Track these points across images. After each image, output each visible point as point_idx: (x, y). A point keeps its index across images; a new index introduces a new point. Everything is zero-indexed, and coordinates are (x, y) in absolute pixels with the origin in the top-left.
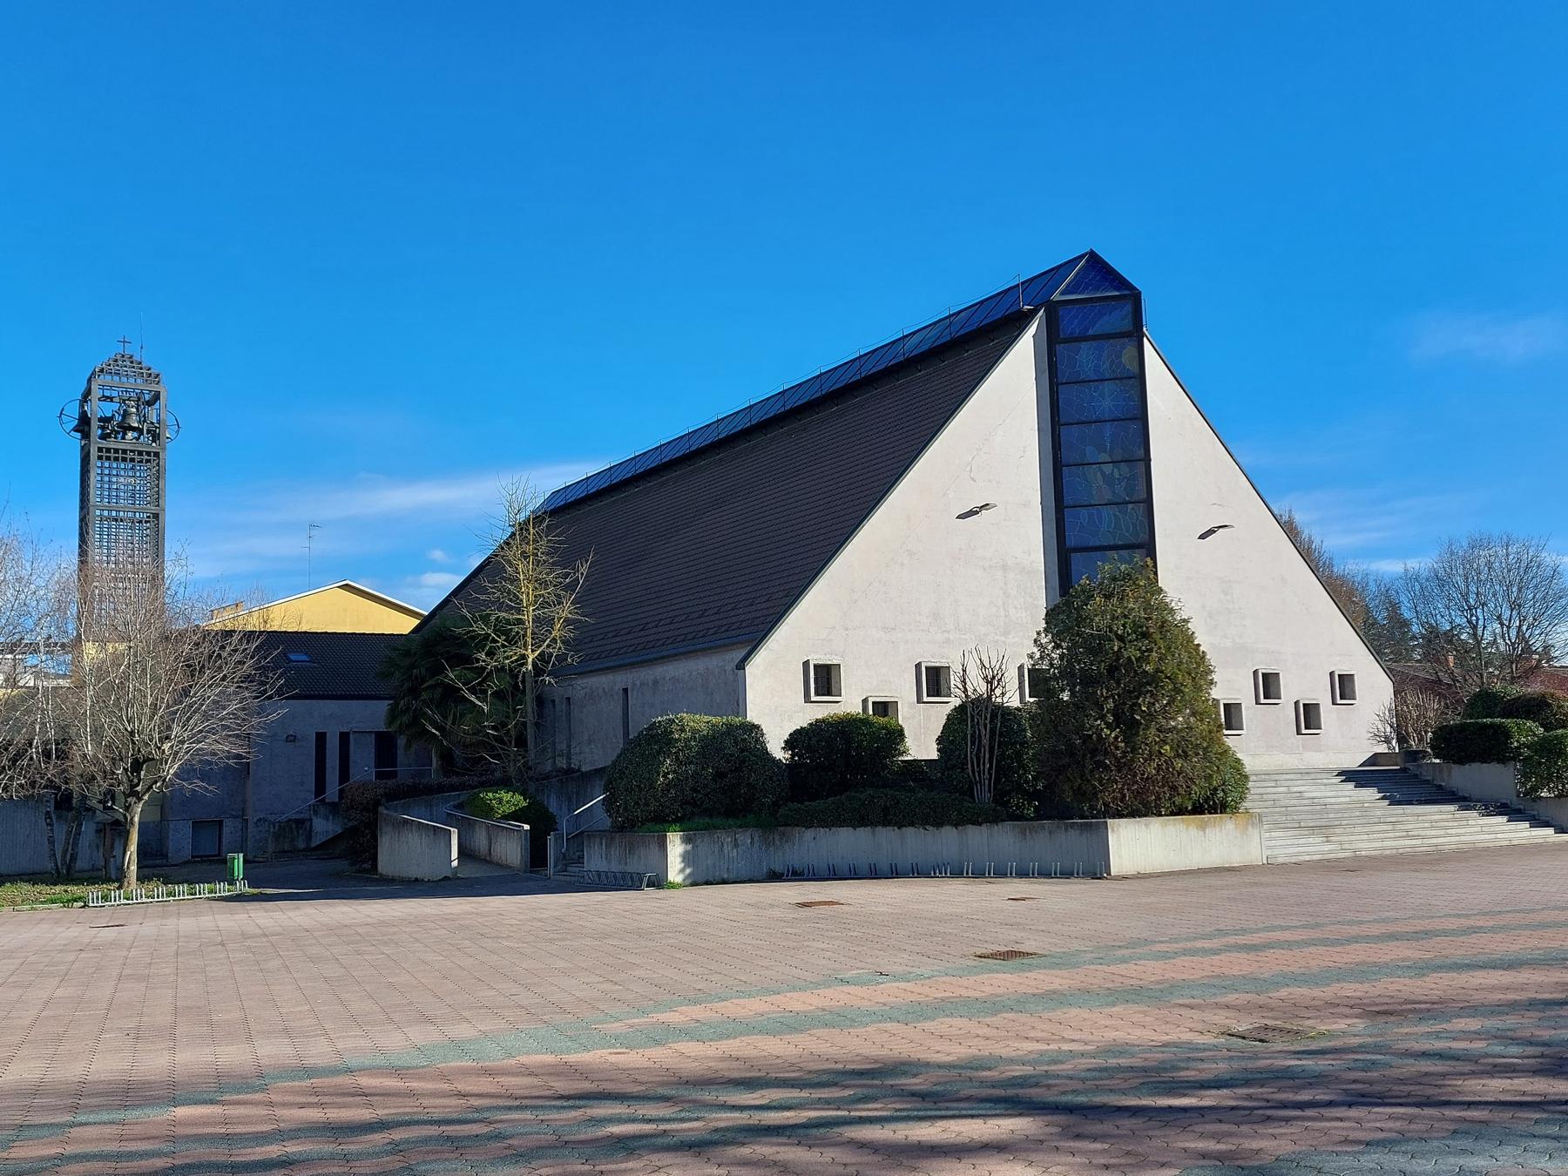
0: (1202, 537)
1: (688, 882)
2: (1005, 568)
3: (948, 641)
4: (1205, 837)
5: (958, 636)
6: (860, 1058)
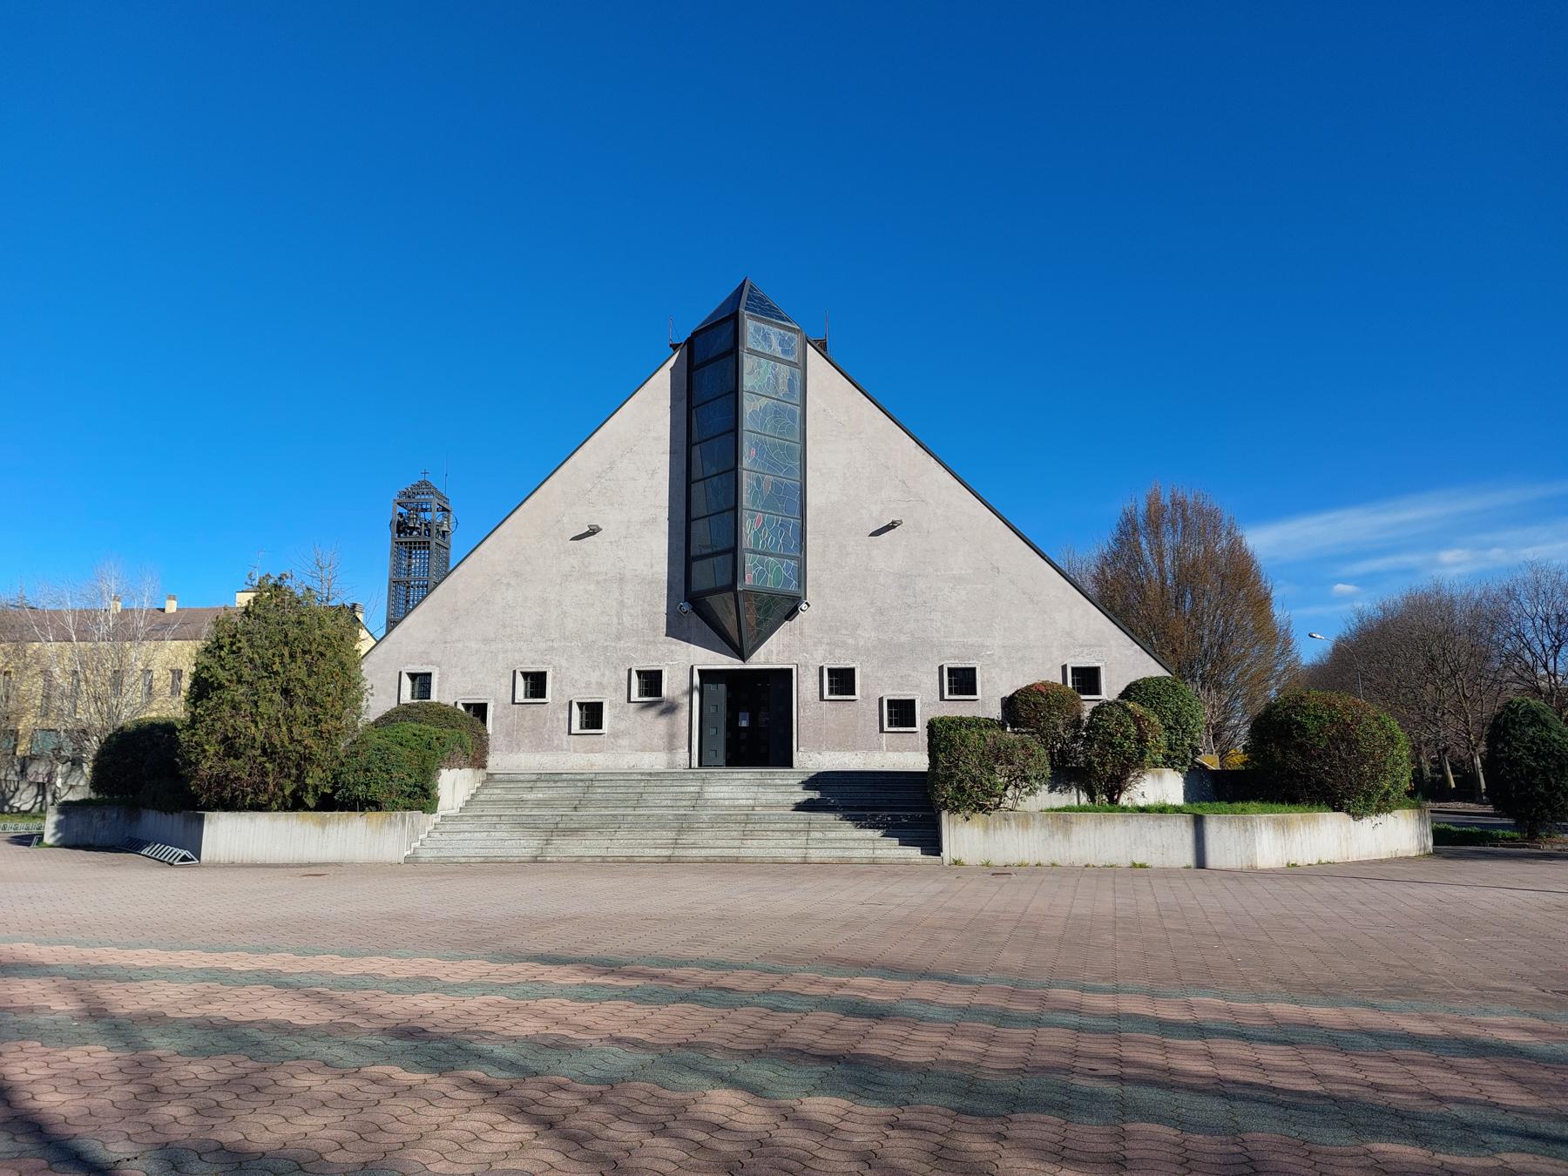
0: (872, 534)
1: (58, 844)
2: (622, 580)
3: (552, 648)
4: (323, 833)
5: (563, 644)
6: (1356, 1027)
